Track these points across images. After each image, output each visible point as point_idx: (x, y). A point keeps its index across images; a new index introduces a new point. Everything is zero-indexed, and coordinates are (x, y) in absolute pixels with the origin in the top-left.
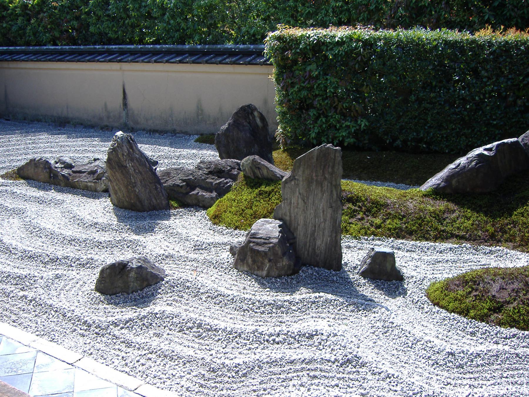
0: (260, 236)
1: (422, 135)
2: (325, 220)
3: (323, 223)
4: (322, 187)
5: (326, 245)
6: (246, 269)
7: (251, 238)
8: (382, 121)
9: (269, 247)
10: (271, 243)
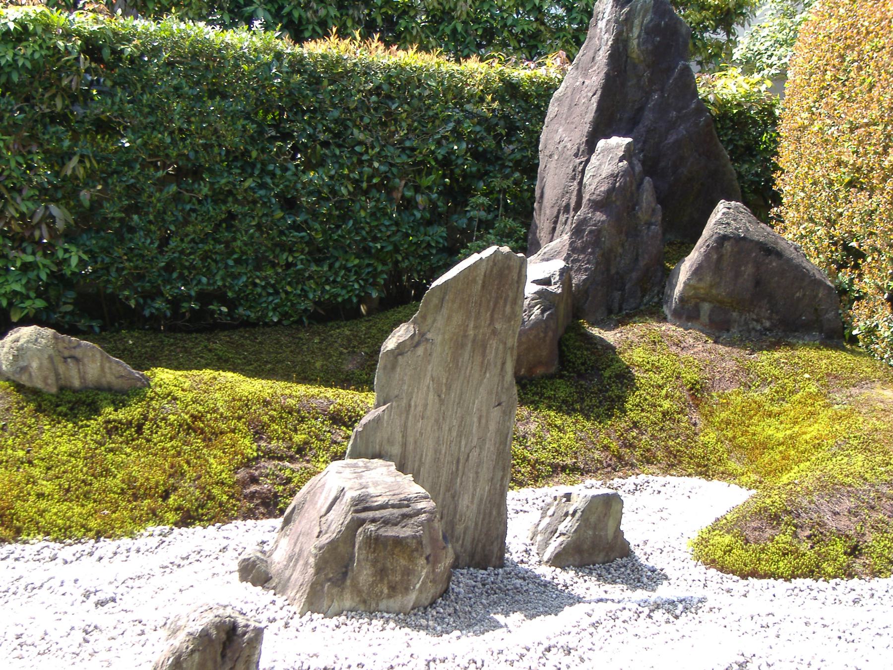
0: (380, 501)
1: (220, 283)
2: (482, 440)
3: (478, 450)
4: (484, 355)
5: (479, 505)
6: (348, 604)
7: (356, 511)
8: (118, 252)
9: (421, 524)
10: (419, 512)
